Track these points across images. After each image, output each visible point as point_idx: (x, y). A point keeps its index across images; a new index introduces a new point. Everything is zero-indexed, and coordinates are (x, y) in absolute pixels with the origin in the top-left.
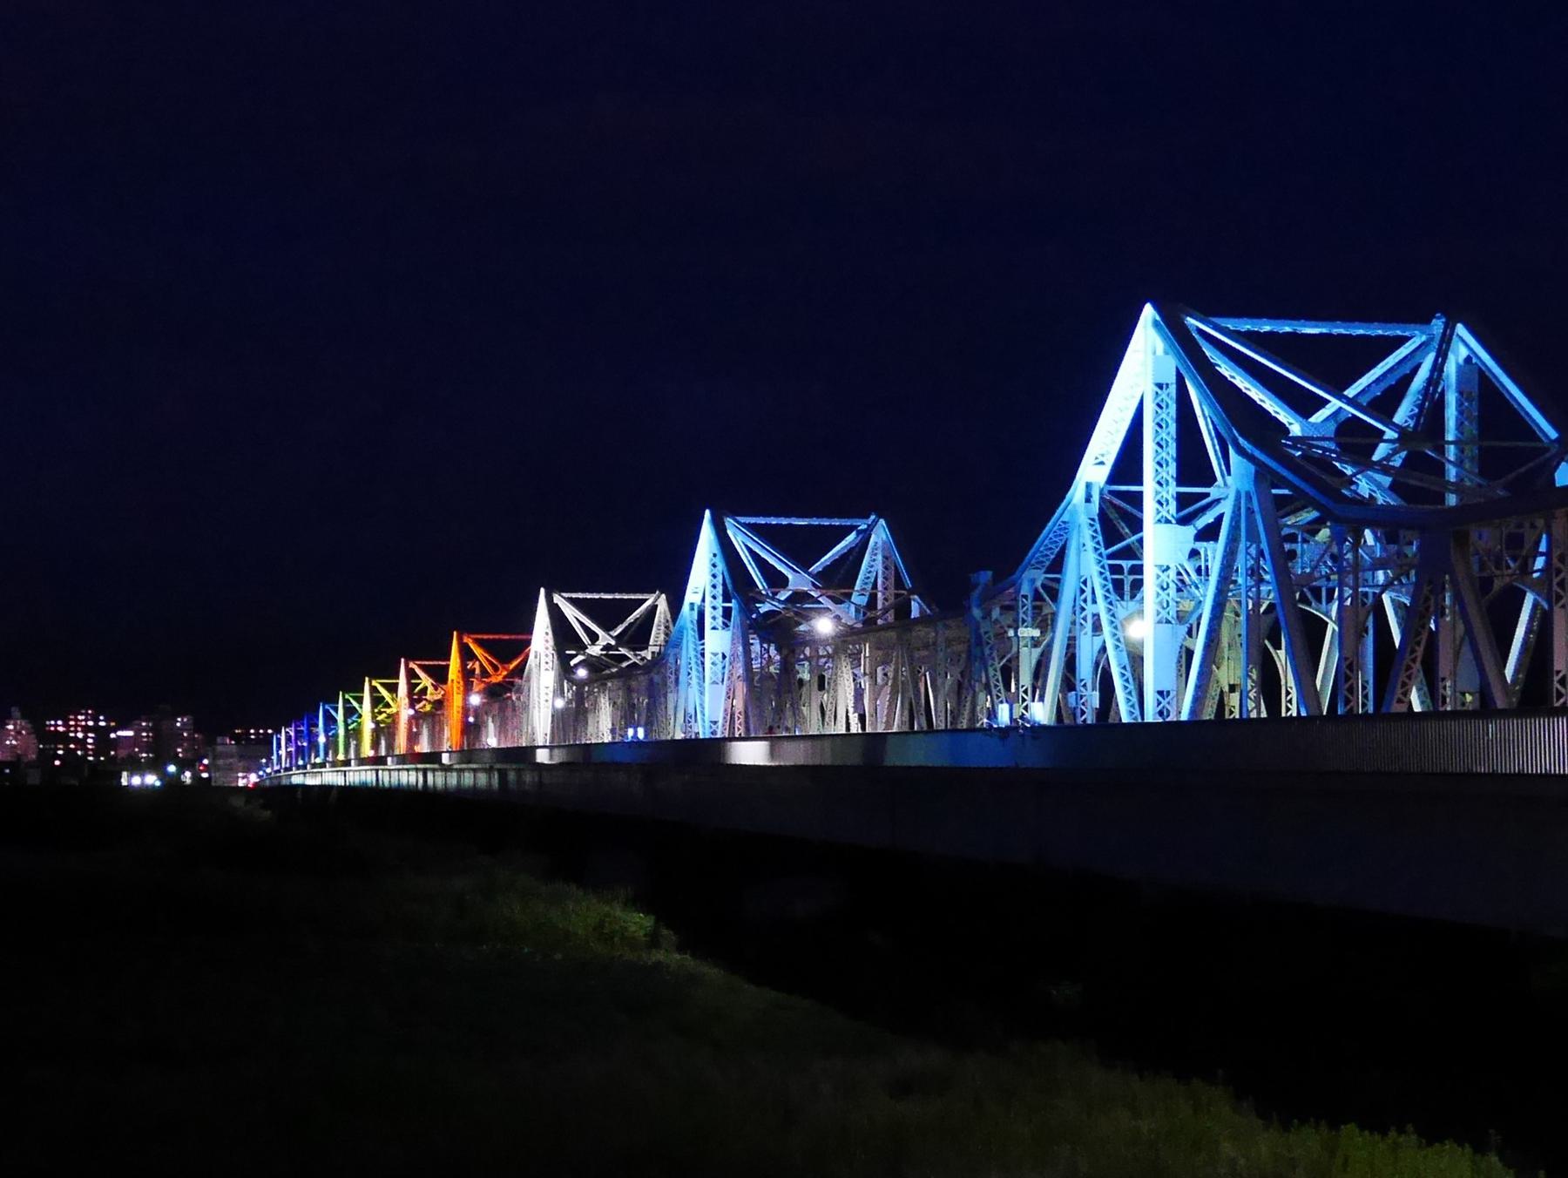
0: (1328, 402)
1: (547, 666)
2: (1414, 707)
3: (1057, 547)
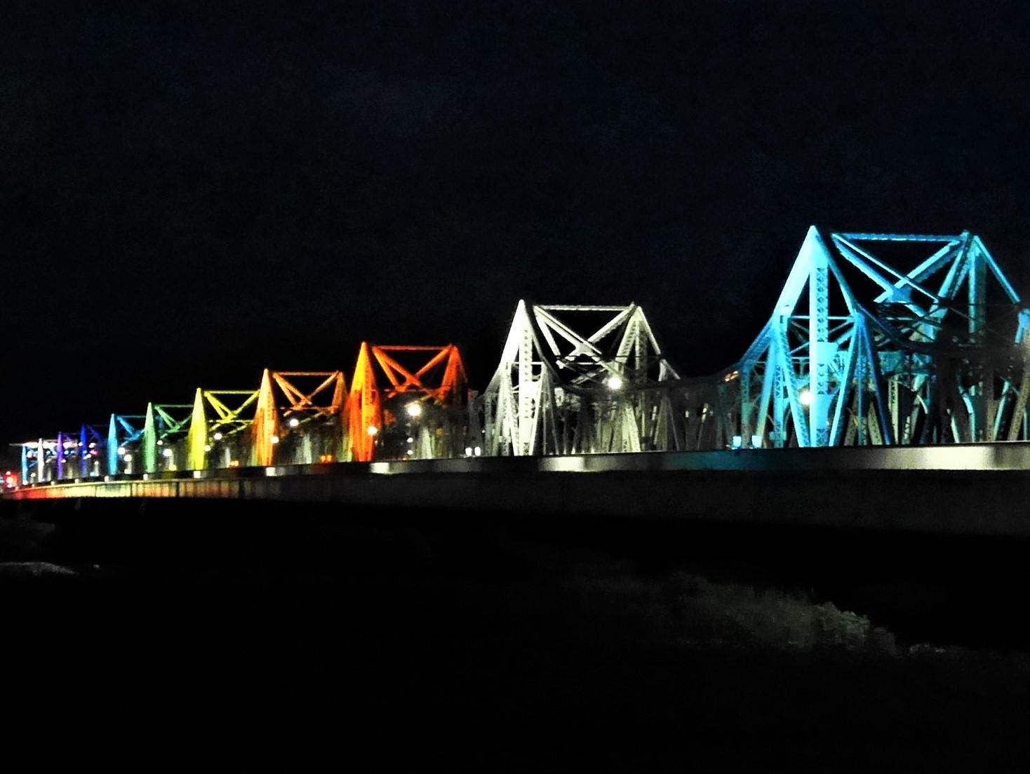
1: (527, 377)
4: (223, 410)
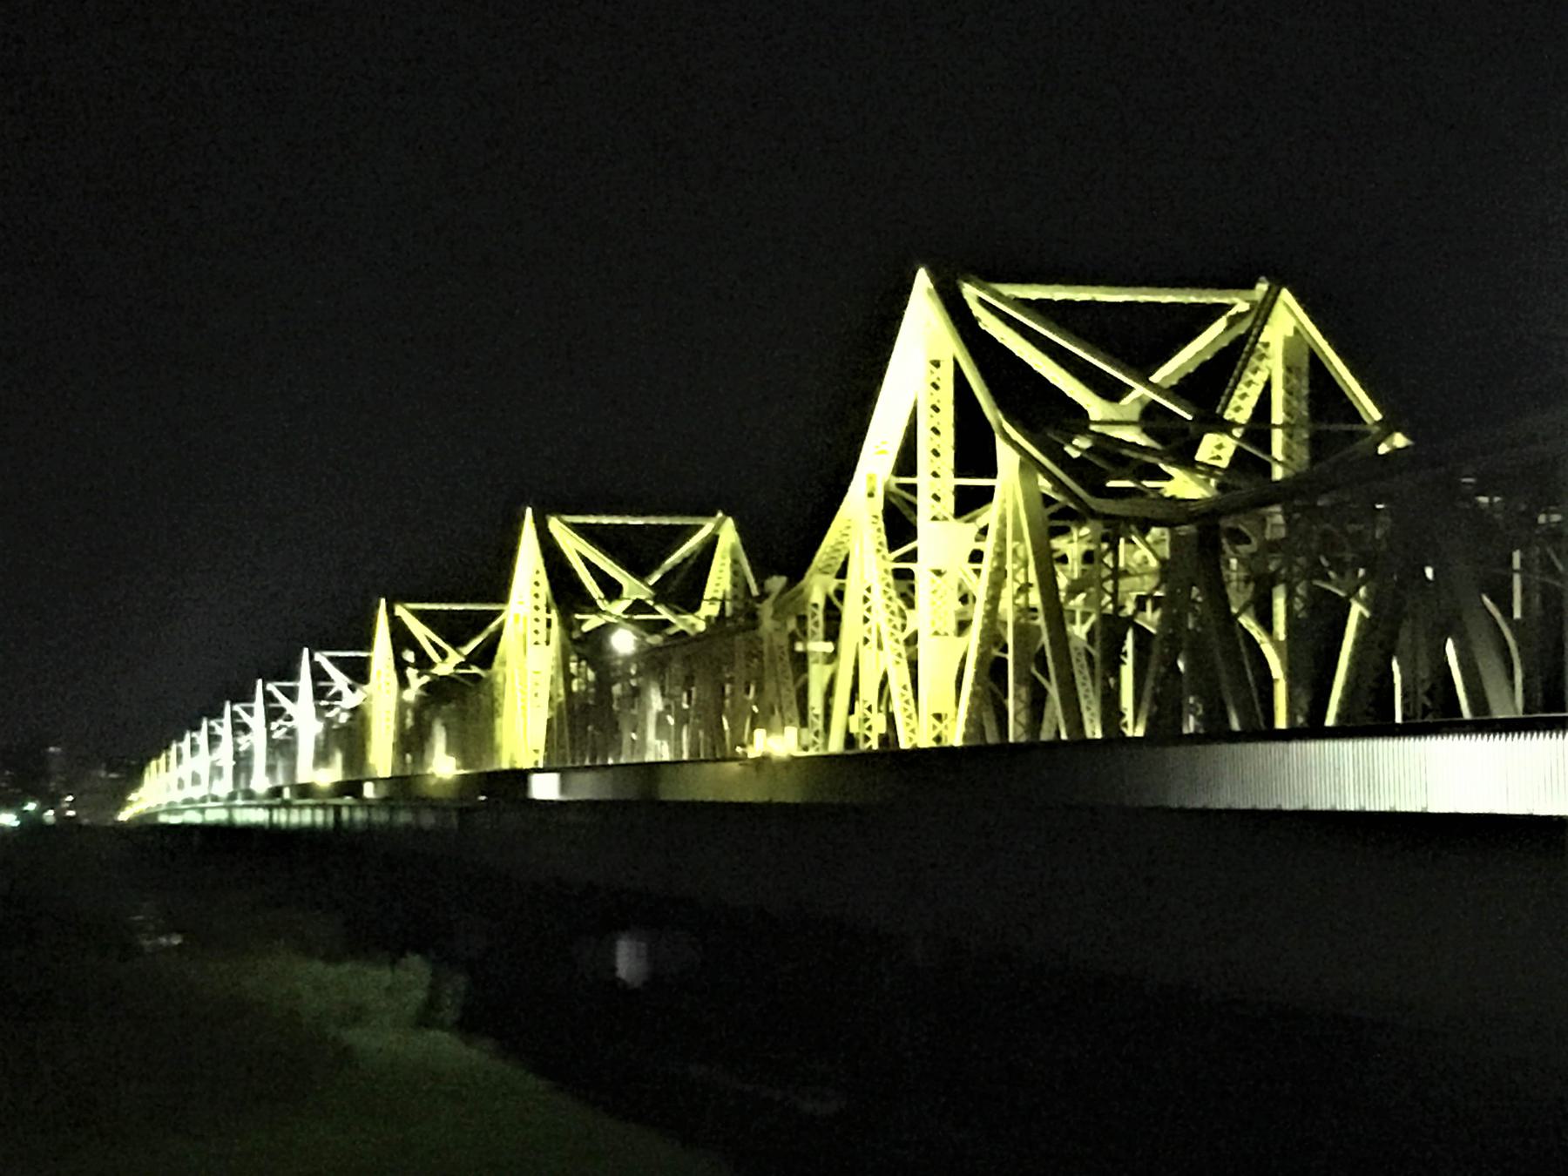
0: (1131, 389)
2: (900, 740)
3: (837, 563)
4: (430, 640)
